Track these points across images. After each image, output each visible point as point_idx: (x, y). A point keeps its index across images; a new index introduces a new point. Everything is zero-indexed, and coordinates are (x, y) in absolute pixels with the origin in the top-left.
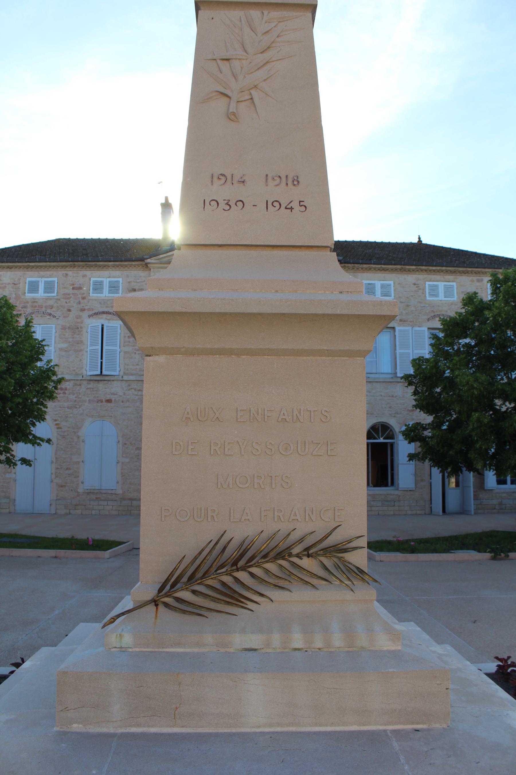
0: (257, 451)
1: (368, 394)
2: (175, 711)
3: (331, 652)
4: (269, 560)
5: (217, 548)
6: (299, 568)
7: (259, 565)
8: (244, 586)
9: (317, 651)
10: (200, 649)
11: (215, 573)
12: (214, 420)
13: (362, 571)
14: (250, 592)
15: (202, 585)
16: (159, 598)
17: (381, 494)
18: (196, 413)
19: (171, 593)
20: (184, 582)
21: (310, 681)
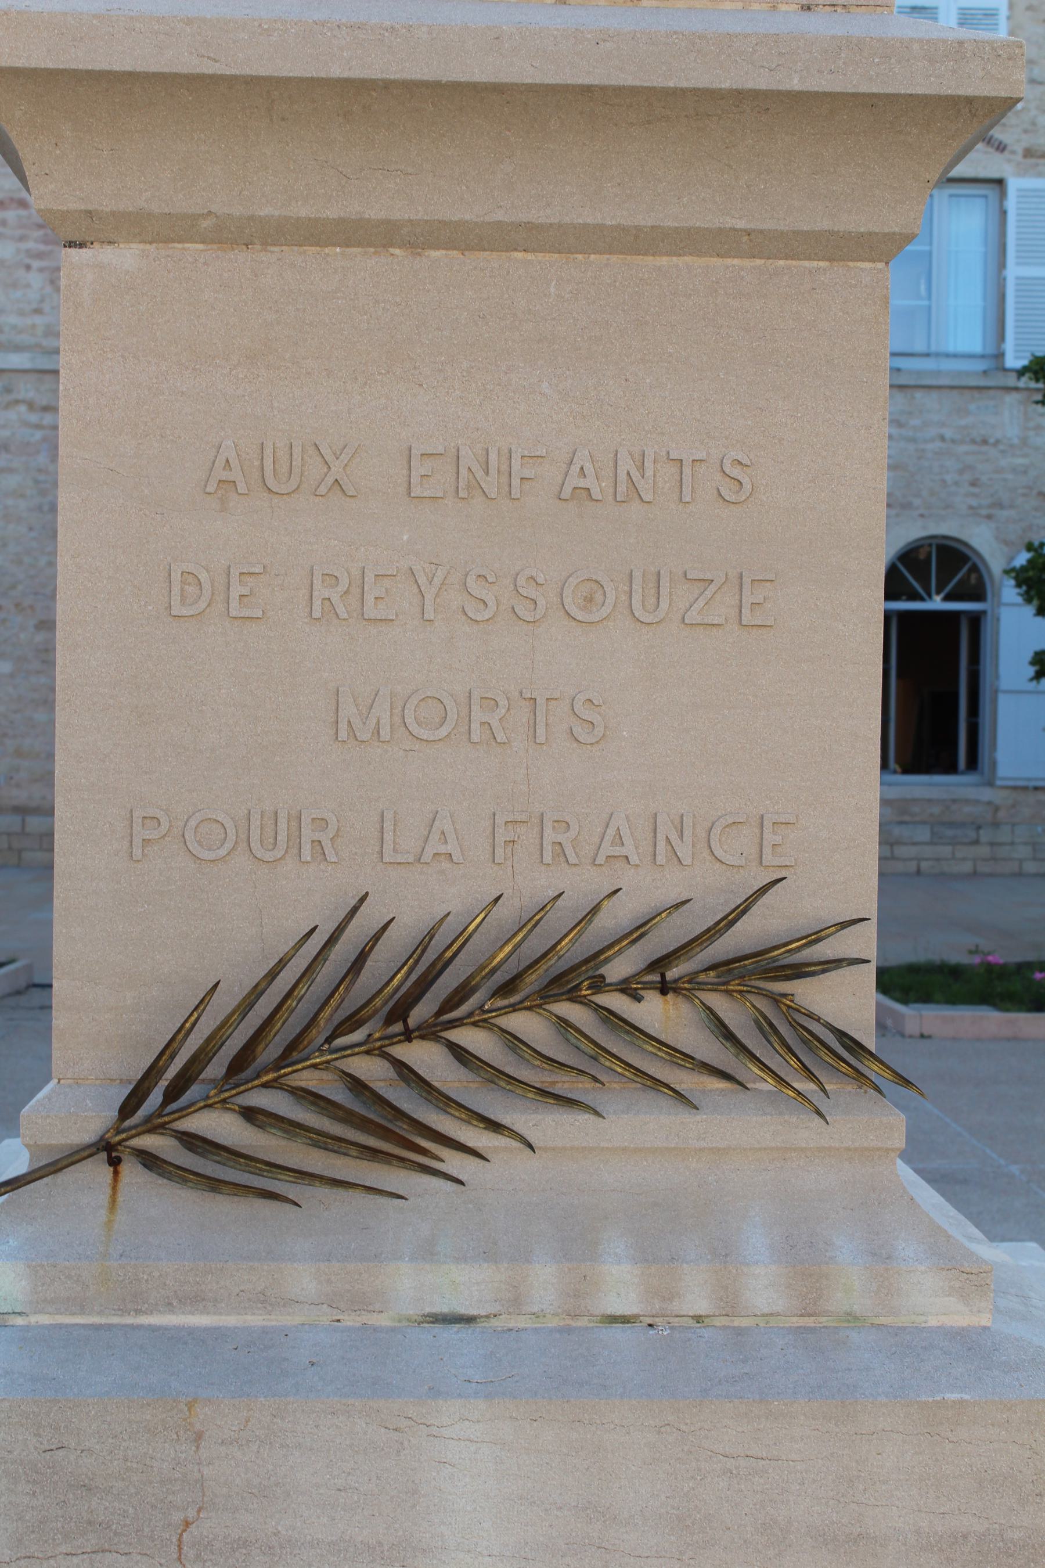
0: (482, 606)
1: (895, 431)
2: (181, 1535)
3: (739, 1332)
4: (521, 1002)
5: (332, 956)
6: (628, 1032)
7: (485, 1020)
8: (429, 1093)
9: (690, 1327)
10: (273, 1317)
11: (327, 1046)
12: (322, 490)
13: (855, 1046)
14: (452, 1115)
15: (281, 1089)
16: (124, 1136)
17: (930, 801)
18: (257, 463)
19: (166, 1119)
20: (213, 1081)
21: (663, 1429)
